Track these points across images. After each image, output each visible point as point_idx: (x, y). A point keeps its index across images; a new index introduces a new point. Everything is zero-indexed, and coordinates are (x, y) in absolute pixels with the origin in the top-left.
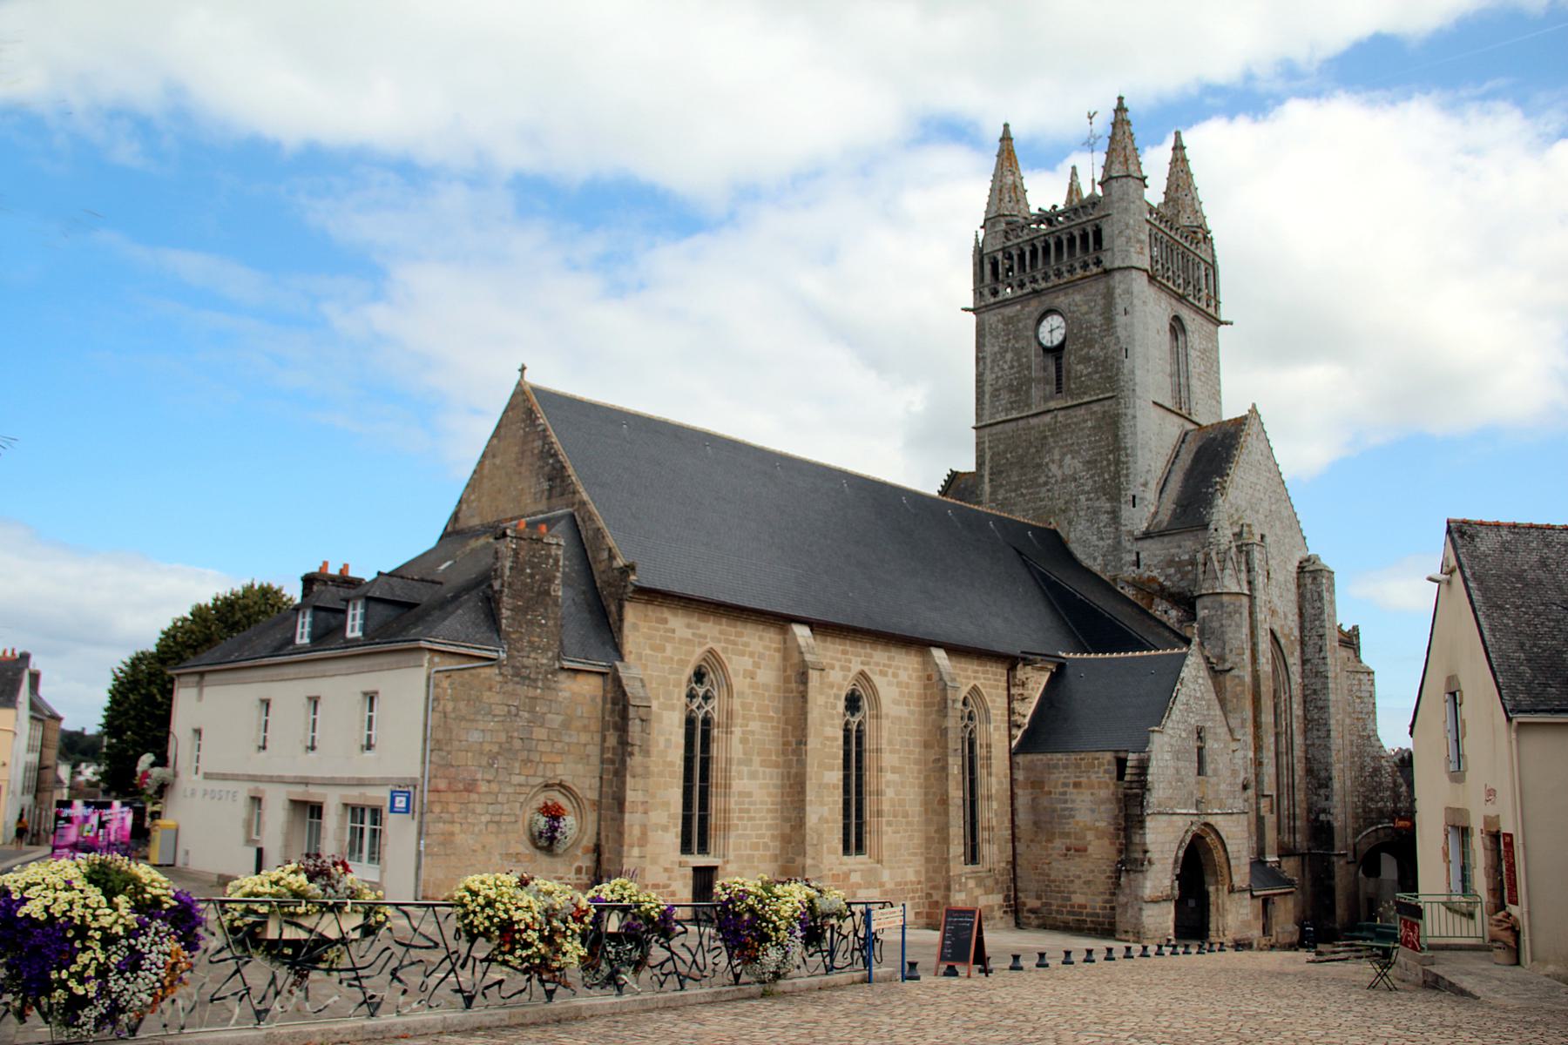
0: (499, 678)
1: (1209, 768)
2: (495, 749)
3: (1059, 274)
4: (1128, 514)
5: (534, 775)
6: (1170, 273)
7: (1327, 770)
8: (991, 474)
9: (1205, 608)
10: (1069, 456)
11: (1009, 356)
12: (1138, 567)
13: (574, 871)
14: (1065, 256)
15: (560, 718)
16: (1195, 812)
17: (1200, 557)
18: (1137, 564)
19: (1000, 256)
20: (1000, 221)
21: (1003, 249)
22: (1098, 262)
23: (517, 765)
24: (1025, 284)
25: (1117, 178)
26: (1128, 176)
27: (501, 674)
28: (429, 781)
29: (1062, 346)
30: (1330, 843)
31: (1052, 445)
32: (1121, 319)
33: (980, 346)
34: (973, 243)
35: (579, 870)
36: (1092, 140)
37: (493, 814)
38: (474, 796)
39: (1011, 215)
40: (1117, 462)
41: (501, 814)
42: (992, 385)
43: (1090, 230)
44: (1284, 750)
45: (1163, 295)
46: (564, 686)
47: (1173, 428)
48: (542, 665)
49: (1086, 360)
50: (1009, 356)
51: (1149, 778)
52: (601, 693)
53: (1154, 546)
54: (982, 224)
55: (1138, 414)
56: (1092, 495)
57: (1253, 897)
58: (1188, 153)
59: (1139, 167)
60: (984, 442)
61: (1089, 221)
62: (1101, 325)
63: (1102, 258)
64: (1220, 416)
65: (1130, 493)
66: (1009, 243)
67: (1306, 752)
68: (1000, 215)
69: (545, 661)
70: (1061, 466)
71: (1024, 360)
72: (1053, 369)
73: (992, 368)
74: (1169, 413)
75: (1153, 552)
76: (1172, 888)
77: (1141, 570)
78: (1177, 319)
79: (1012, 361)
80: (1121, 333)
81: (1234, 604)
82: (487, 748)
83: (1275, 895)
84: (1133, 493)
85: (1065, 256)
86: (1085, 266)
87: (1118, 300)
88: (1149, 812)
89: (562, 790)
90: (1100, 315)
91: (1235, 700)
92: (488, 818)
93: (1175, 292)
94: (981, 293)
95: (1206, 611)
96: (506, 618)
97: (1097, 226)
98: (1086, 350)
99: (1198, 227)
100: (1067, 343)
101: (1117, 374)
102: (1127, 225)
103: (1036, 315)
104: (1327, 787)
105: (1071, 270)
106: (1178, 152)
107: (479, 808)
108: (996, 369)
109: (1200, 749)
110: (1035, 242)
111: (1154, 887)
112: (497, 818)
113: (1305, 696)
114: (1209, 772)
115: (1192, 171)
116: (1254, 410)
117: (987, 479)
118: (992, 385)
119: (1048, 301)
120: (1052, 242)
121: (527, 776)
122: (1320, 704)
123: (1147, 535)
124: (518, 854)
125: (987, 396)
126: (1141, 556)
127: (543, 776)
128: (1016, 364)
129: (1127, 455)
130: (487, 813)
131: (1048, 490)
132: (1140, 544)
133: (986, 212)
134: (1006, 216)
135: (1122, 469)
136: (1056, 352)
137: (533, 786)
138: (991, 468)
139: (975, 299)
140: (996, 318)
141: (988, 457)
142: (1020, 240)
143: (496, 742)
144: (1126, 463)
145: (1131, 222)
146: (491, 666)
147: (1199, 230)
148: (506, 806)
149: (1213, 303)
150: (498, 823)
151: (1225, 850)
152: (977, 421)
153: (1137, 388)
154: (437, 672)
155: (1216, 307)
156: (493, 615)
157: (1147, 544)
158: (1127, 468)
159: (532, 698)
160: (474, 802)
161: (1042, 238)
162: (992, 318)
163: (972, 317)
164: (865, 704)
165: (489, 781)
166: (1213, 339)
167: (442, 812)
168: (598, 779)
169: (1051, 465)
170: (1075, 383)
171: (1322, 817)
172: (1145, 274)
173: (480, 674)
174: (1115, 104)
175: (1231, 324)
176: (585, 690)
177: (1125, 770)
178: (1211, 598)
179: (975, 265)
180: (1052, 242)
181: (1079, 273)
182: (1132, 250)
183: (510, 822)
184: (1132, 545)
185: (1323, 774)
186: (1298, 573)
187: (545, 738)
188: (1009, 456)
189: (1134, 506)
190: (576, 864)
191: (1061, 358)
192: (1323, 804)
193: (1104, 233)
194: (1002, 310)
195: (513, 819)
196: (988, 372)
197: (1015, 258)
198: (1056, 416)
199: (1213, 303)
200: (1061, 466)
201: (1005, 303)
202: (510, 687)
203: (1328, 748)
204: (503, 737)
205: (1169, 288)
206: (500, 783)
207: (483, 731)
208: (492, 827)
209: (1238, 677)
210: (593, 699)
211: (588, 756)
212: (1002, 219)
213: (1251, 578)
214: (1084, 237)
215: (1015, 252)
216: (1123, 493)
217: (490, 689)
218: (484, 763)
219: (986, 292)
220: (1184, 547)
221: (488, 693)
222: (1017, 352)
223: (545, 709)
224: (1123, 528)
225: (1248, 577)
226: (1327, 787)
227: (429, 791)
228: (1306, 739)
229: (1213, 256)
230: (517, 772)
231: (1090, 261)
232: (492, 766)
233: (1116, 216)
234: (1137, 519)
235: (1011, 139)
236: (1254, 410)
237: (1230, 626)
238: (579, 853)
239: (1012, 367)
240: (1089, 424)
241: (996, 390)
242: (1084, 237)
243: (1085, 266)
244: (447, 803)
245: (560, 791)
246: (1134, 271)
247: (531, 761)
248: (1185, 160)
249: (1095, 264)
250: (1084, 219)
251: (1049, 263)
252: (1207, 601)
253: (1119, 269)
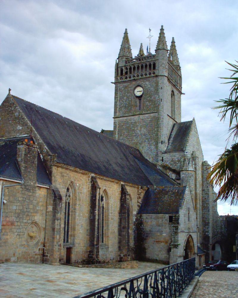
0: (21, 189)
1: (190, 219)
2: (19, 211)
3: (142, 75)
4: (160, 146)
5: (29, 220)
7: (208, 221)
8: (118, 132)
9: (183, 174)
10: (143, 128)
11: (125, 98)
12: (163, 161)
13: (38, 249)
14: (140, 71)
15: (36, 202)
16: (187, 231)
17: (182, 160)
18: (163, 160)
19: (124, 68)
20: (124, 58)
21: (125, 66)
22: (154, 73)
23: (25, 216)
24: (127, 78)
25: (161, 49)
26: (164, 49)
27: (21, 188)
28: (2, 222)
29: (141, 96)
30: (208, 241)
31: (138, 124)
32: (160, 90)
33: (116, 94)
34: (115, 63)
35: (39, 249)
36: (150, 37)
37: (18, 232)
38: (13, 227)
39: (127, 56)
40: (158, 131)
41: (20, 232)
42: (120, 106)
43: (152, 64)
45: (170, 84)
46: (37, 192)
47: (171, 122)
48: (32, 185)
49: (150, 101)
50: (125, 98)
51: (180, 222)
52: (46, 194)
53: (167, 156)
54: (117, 57)
55: (164, 118)
56: (150, 140)
57: (198, 255)
58: (176, 44)
59: (167, 47)
60: (116, 122)
61: (152, 61)
62: (154, 91)
63: (155, 72)
64: (181, 121)
65: (161, 140)
66: (127, 65)
67: (203, 215)
68: (124, 56)
69: (33, 184)
70: (140, 131)
71: (130, 99)
72: (138, 103)
73: (119, 101)
74: (170, 118)
75: (166, 157)
76: (183, 253)
77: (163, 162)
78: (173, 91)
79: (126, 99)
80: (160, 94)
81: (192, 173)
82: (17, 211)
83: (202, 255)
84: (162, 140)
85: (140, 71)
86: (150, 74)
87: (160, 85)
88: (180, 231)
89: (36, 225)
90: (154, 88)
92: (16, 234)
94: (117, 78)
95: (184, 175)
96: (23, 170)
97: (154, 62)
98: (149, 98)
99: (178, 66)
100: (143, 95)
101: (158, 106)
102: (163, 63)
103: (134, 87)
104: (208, 225)
105: (146, 75)
106: (173, 43)
107: (15, 231)
108: (121, 101)
109: (189, 214)
110: (135, 65)
111: (180, 253)
112: (19, 234)
113: (202, 200)
114: (190, 221)
115: (177, 50)
116: (194, 119)
117: (117, 134)
118: (120, 106)
119: (138, 82)
120: (140, 66)
121: (27, 220)
122: (207, 202)
123: (166, 152)
124: (24, 245)
125: (118, 109)
126: (164, 158)
127: (31, 220)
128: (127, 100)
129: (160, 129)
130: (17, 232)
131: (136, 138)
132: (163, 155)
133: (119, 54)
134: (126, 56)
136: (140, 98)
137: (29, 223)
138: (118, 130)
139: (115, 80)
140: (121, 86)
141: (117, 127)
142: (130, 64)
143: (20, 209)
145: (164, 63)
146: (19, 185)
147: (178, 67)
148: (22, 230)
149: (180, 88)
150: (20, 235)
151: (193, 242)
152: (114, 116)
153: (164, 110)
154: (5, 187)
155: (181, 89)
156: (17, 168)
157: (165, 155)
158: (160, 133)
159: (29, 195)
160: (13, 229)
161: (137, 64)
162: (121, 86)
163: (114, 85)
164: (104, 198)
165: (17, 222)
166: (180, 98)
167: (5, 232)
168: (45, 221)
169: (137, 130)
170: (145, 107)
171: (207, 233)
172: (167, 78)
173: (16, 188)
174: (160, 28)
175: (185, 94)
176: (41, 193)
177: (172, 219)
178: (185, 171)
179: (115, 70)
180: (140, 66)
181: (140, 77)
182: (164, 70)
183: (23, 235)
184: (161, 155)
185: (207, 221)
186: (202, 166)
187: (32, 208)
188: (124, 127)
189: (162, 144)
190: (39, 248)
191: (141, 99)
192: (207, 230)
193: (157, 65)
194: (124, 84)
195: (23, 234)
196: (118, 102)
197: (128, 69)
198: (139, 117)
199: (180, 88)
200: (140, 131)
201: (124, 82)
202: (23, 192)
203: (209, 215)
204: (21, 208)
206: (20, 222)
207: (16, 206)
208: (18, 237)
210: (45, 195)
211: (43, 214)
212: (125, 57)
213: (196, 167)
214: (150, 65)
215: (128, 68)
216: (159, 140)
217: (18, 193)
218: (16, 216)
219: (119, 78)
220: (177, 156)
221: (18, 194)
222: (128, 98)
223: (32, 199)
224: (159, 150)
225: (195, 166)
226: (208, 225)
227: (2, 225)
228: (203, 212)
229: (181, 74)
230: (25, 219)
231: (147, 73)
232: (18, 217)
233: (160, 61)
234: (163, 147)
235: (128, 34)
236: (194, 119)
237: (191, 180)
238: (40, 244)
239: (126, 101)
240: (149, 119)
241: (121, 107)
242: (150, 65)
243: (150, 74)
244: (6, 229)
245: (35, 225)
246: (164, 77)
247: (29, 215)
248: (175, 46)
249: (153, 73)
250: (150, 60)
251: (147, 70)
252: (184, 172)
253: (160, 76)
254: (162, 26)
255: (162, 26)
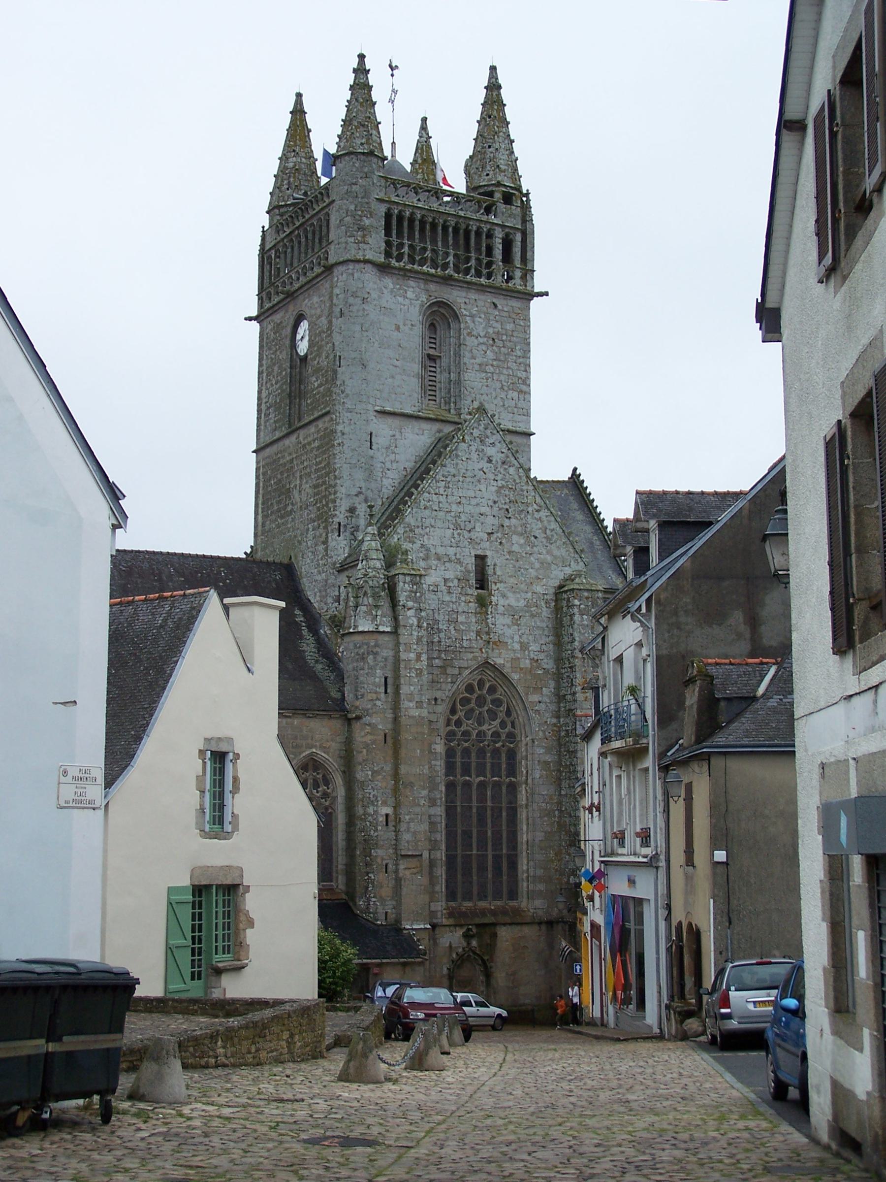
6: (428, 254)
44: (524, 802)
81: (368, 644)
84: (338, 520)
91: (365, 751)
93: (432, 275)
129: (336, 477)
135: (330, 494)
144: (335, 485)
158: (335, 493)
172: (369, 267)
174: (355, 63)
175: (546, 294)
189: (339, 535)
205: (416, 272)
209: (369, 725)
240: (316, 444)
246: (351, 266)
254: (362, 57)
255: (362, 57)
